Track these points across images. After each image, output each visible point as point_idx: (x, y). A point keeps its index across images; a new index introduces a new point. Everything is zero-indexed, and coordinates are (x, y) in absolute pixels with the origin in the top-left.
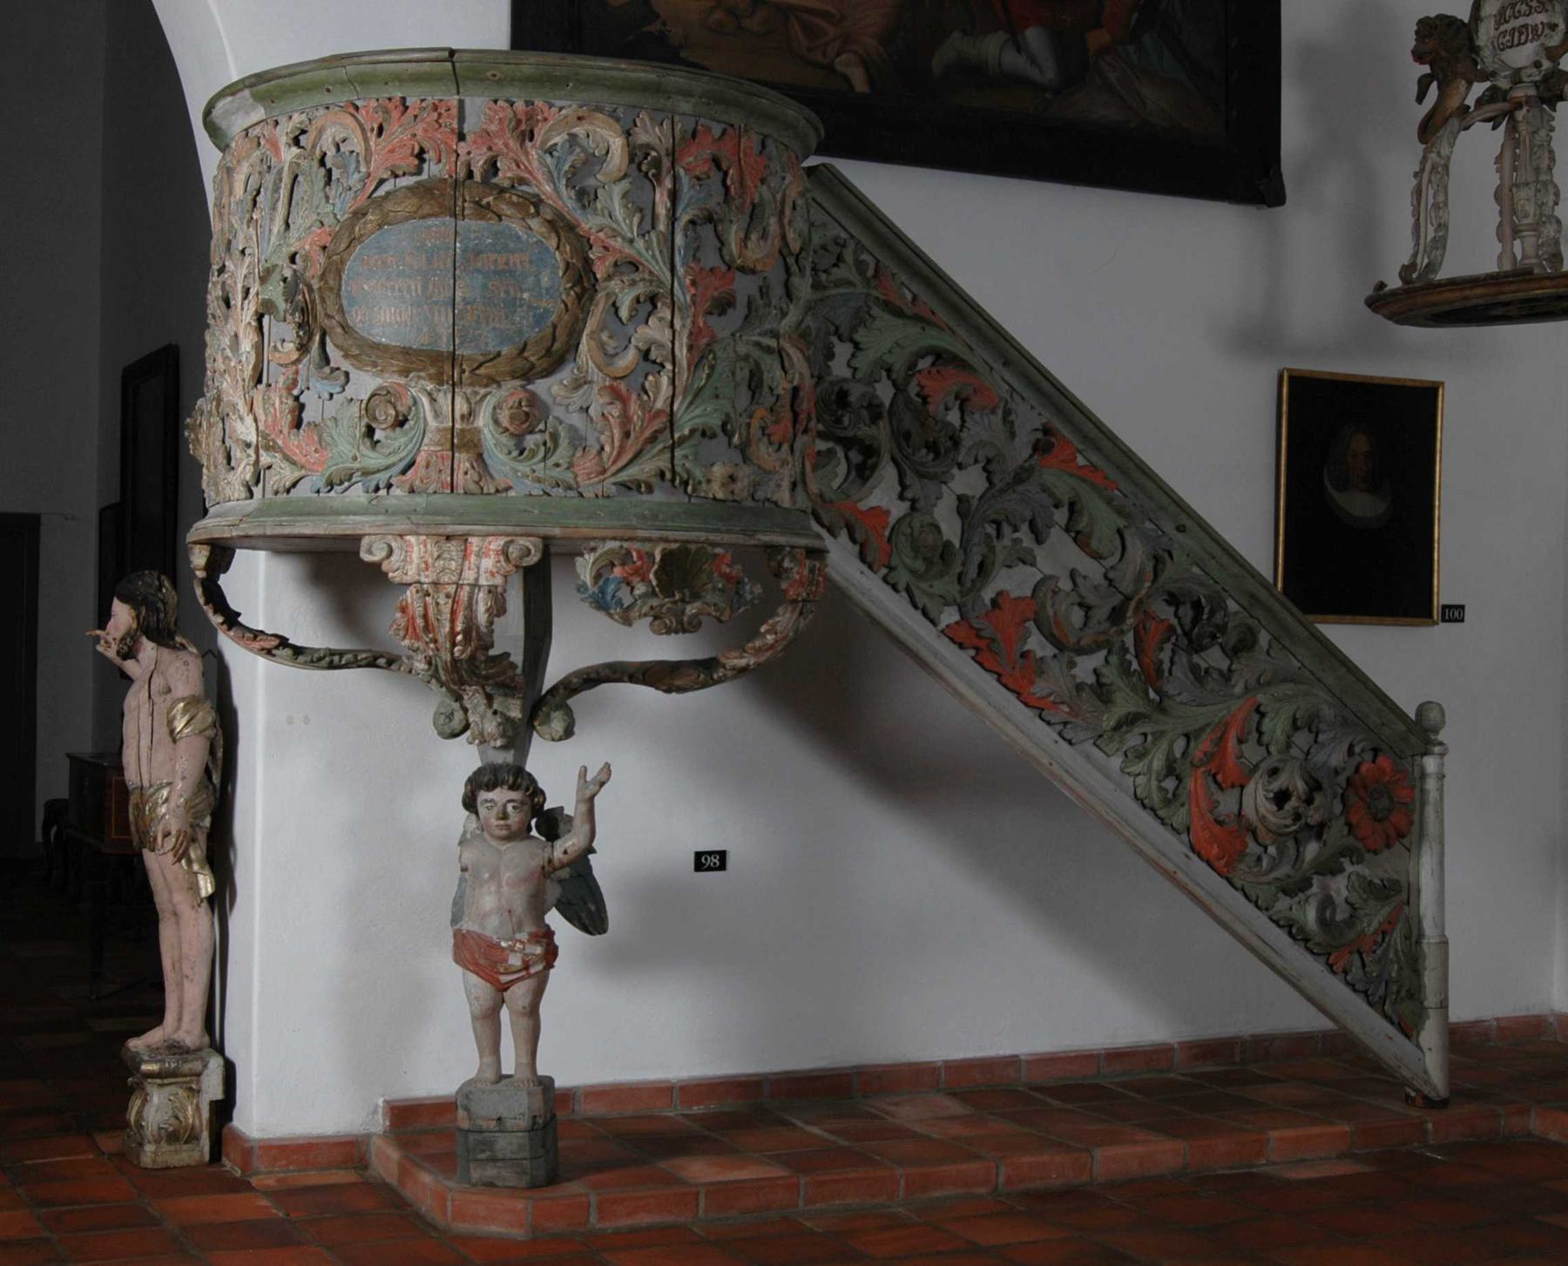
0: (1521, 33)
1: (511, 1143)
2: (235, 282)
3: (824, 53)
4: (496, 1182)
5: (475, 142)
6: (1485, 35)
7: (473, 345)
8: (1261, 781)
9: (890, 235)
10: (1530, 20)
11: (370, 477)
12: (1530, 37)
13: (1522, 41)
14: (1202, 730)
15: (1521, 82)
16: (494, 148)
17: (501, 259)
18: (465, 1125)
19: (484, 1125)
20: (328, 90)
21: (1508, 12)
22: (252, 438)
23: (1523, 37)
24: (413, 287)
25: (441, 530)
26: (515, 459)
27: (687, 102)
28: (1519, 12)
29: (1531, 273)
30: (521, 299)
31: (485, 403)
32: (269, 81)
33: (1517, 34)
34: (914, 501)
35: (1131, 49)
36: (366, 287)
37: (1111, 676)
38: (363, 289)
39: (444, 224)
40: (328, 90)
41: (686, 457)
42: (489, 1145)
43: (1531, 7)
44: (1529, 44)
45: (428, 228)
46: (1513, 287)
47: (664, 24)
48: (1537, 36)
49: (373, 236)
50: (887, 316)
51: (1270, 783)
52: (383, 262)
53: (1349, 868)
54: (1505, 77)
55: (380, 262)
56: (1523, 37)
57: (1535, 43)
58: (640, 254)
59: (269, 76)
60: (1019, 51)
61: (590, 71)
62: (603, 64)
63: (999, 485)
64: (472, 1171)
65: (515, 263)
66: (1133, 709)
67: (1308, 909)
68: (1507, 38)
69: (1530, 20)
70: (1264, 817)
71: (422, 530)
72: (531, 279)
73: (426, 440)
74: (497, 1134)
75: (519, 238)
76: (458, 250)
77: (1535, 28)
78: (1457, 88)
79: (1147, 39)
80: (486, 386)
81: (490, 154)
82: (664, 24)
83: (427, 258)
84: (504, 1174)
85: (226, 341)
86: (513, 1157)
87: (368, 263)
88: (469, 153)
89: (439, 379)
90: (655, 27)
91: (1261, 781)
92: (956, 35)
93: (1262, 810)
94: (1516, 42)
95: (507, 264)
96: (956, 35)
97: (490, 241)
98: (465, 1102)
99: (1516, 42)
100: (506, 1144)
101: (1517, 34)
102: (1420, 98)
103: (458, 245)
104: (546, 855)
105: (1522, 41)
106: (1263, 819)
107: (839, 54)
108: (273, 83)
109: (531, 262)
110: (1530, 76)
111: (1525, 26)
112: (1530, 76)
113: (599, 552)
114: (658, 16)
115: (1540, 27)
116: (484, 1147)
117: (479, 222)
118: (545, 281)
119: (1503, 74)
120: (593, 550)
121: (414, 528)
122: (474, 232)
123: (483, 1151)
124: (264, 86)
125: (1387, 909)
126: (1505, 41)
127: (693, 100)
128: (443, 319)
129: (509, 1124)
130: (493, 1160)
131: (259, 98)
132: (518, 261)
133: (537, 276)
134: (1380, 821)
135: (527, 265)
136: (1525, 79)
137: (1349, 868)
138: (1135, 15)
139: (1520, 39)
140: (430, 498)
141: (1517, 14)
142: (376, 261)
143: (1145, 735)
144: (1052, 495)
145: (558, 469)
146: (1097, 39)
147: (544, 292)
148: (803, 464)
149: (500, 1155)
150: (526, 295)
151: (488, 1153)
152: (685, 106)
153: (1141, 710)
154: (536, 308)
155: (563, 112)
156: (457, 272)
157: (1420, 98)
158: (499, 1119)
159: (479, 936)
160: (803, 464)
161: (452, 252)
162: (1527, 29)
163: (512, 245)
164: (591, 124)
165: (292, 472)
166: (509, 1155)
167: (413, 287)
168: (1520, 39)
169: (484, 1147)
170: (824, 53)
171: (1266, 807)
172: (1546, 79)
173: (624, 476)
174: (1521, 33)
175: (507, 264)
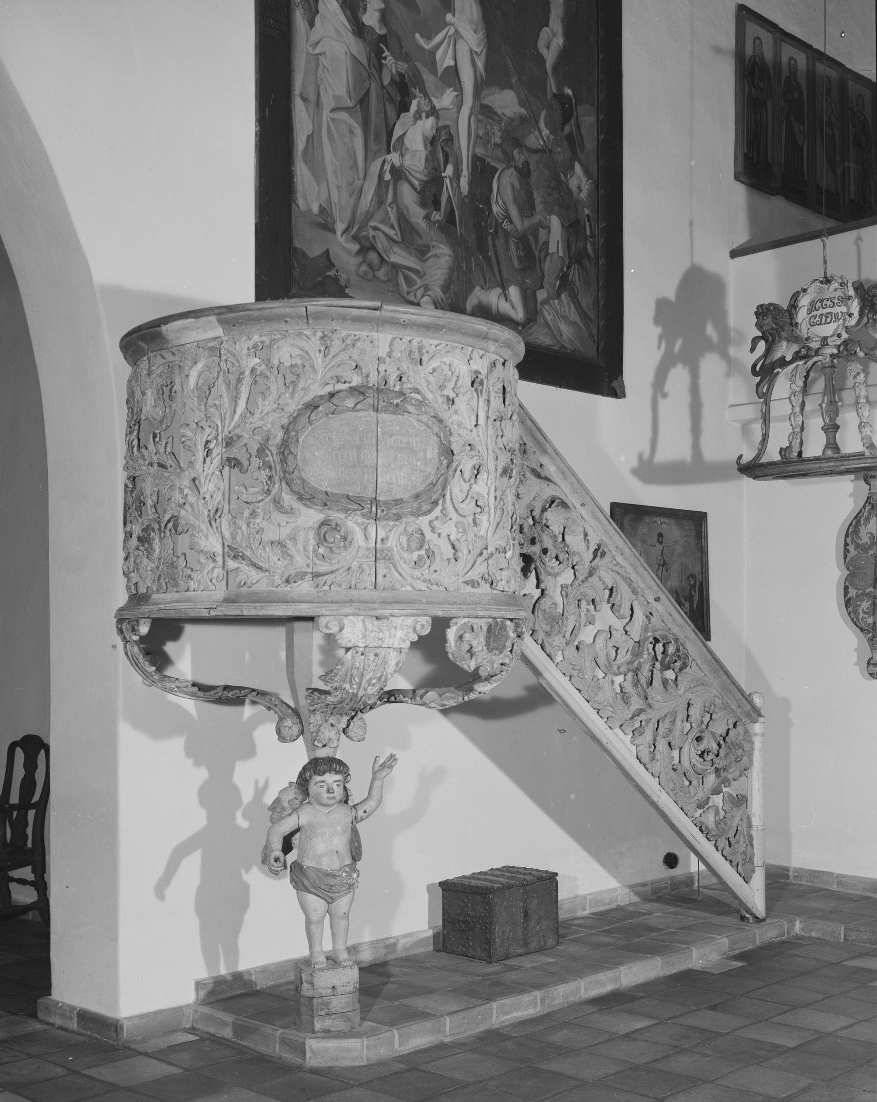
0: (827, 317)
1: (340, 1003)
2: (195, 444)
3: (415, 296)
4: (331, 1029)
5: (390, 364)
6: (802, 316)
7: (387, 494)
8: (692, 744)
10: (833, 310)
11: (320, 578)
12: (834, 319)
13: (828, 321)
14: (666, 716)
15: (828, 344)
16: (401, 369)
17: (405, 440)
19: (323, 992)
20: (286, 322)
21: (818, 305)
22: (218, 549)
23: (829, 320)
24: (351, 456)
25: (374, 613)
27: (494, 345)
28: (826, 305)
29: (864, 455)
30: (417, 466)
31: (393, 531)
33: (824, 318)
35: (556, 301)
36: (317, 454)
37: (629, 688)
38: (314, 455)
39: (370, 415)
41: (493, 565)
42: (327, 1005)
43: (834, 303)
44: (832, 324)
47: (337, 271)
48: (837, 319)
49: (321, 421)
51: (698, 745)
52: (329, 439)
54: (816, 342)
55: (327, 439)
56: (829, 320)
57: (836, 324)
58: (474, 439)
64: (315, 1023)
65: (412, 443)
66: (639, 707)
67: (709, 815)
69: (833, 310)
70: (694, 765)
72: (422, 453)
73: (360, 555)
74: (332, 997)
76: (379, 433)
77: (836, 315)
78: (782, 346)
79: (563, 297)
82: (337, 271)
83: (360, 437)
85: (186, 482)
86: (342, 1011)
87: (318, 439)
88: (386, 371)
90: (332, 273)
91: (692, 744)
93: (694, 761)
94: (823, 322)
95: (408, 443)
96: (478, 288)
97: (397, 428)
98: (310, 978)
99: (823, 322)
100: (337, 1004)
101: (824, 318)
102: (752, 350)
103: (379, 430)
104: (354, 815)
105: (828, 321)
106: (693, 766)
108: (241, 313)
109: (421, 442)
110: (833, 341)
111: (830, 313)
112: (833, 341)
113: (459, 624)
114: (333, 265)
116: (323, 1007)
117: (391, 415)
118: (429, 456)
119: (815, 340)
122: (389, 421)
123: (323, 1009)
125: (741, 812)
126: (815, 321)
127: (497, 344)
129: (340, 990)
130: (329, 1014)
131: (223, 322)
132: (414, 442)
133: (425, 451)
135: (419, 444)
136: (830, 343)
137: (725, 790)
138: (558, 283)
139: (826, 320)
140: (360, 592)
141: (824, 306)
142: (325, 437)
143: (641, 722)
145: (436, 574)
146: (542, 295)
147: (428, 461)
150: (419, 463)
152: (492, 348)
153: (642, 707)
154: (424, 472)
155: (438, 348)
157: (752, 350)
158: (333, 987)
159: (317, 870)
161: (375, 433)
163: (410, 431)
165: (257, 574)
166: (340, 1010)
167: (351, 456)
168: (826, 320)
169: (323, 1007)
170: (415, 296)
173: (467, 578)
174: (827, 317)
175: (408, 443)
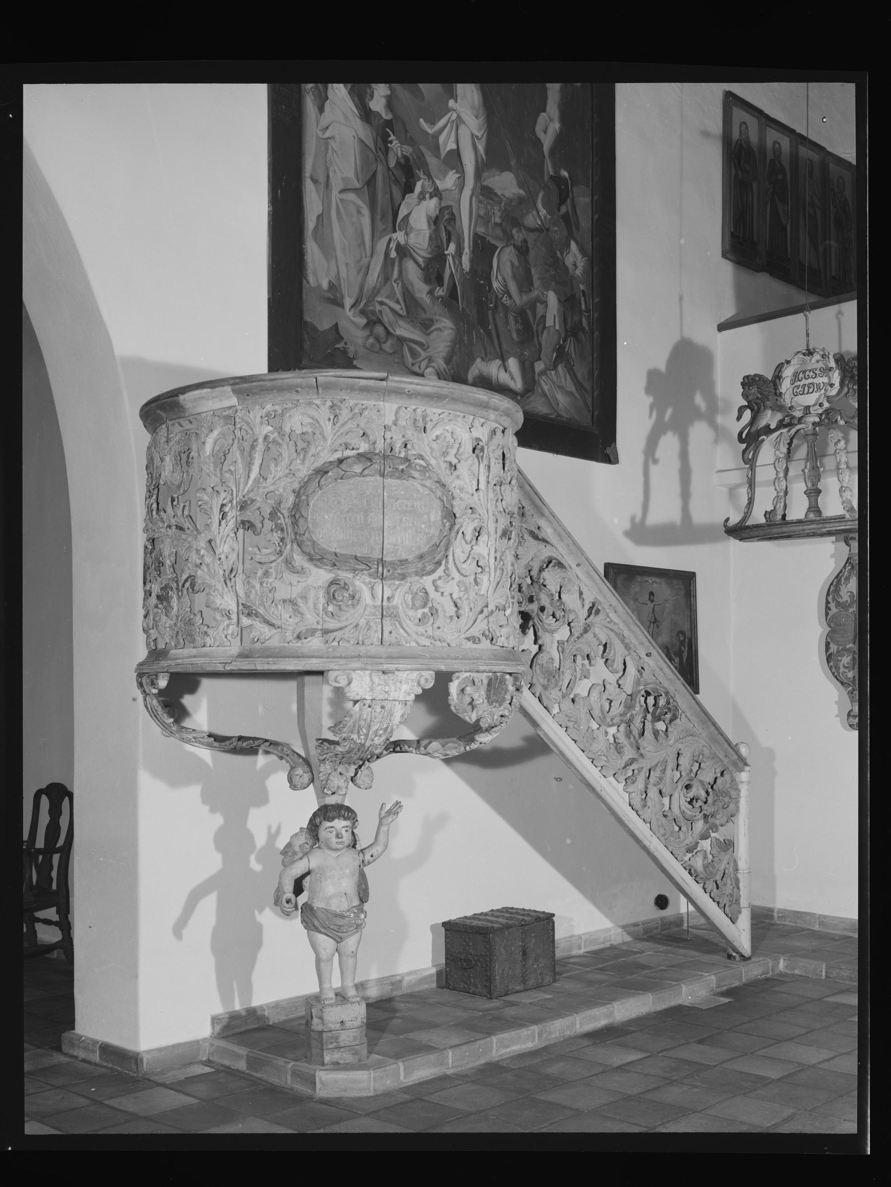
0: (809, 388)
3: (419, 367)
4: (340, 1062)
9: (532, 492)
10: (815, 381)
16: (406, 436)
18: (320, 1028)
19: (333, 1026)
20: (297, 391)
21: (801, 375)
23: (811, 390)
24: (358, 518)
26: (416, 624)
28: (808, 376)
29: (844, 518)
30: (421, 528)
32: (252, 382)
33: (806, 388)
34: (540, 647)
35: (553, 372)
36: (326, 517)
40: (297, 391)
42: (336, 1039)
43: (816, 374)
44: (814, 394)
45: (368, 482)
46: (832, 525)
47: (346, 344)
48: (819, 389)
50: (531, 539)
51: (688, 793)
52: (338, 502)
53: (713, 835)
54: (799, 410)
55: (336, 503)
56: (811, 390)
57: (818, 394)
59: (254, 379)
60: (506, 371)
61: (413, 386)
62: (415, 381)
63: (577, 634)
64: (325, 1056)
68: (800, 389)
69: (815, 381)
71: (369, 667)
72: (426, 516)
75: (418, 491)
76: (385, 497)
77: (818, 385)
78: (766, 415)
79: (560, 368)
80: (375, 579)
81: (403, 439)
82: (346, 344)
84: (344, 1055)
86: (350, 1044)
89: (375, 575)
90: (340, 345)
91: (682, 792)
92: (479, 360)
93: (683, 808)
95: (413, 506)
100: (345, 1038)
102: (739, 418)
103: (385, 494)
106: (683, 813)
107: (426, 368)
108: (254, 384)
110: (816, 410)
111: (813, 384)
112: (816, 410)
114: (342, 338)
115: (822, 385)
116: (332, 1041)
118: (433, 519)
120: (458, 677)
121: (364, 666)
123: (332, 1043)
124: (246, 385)
126: (798, 391)
128: (377, 539)
130: (339, 1048)
133: (429, 514)
134: (725, 808)
136: (812, 412)
137: (713, 835)
139: (809, 390)
142: (334, 501)
143: (633, 770)
144: (598, 639)
145: (439, 630)
146: (539, 366)
148: (406, 631)
149: (342, 1044)
150: (423, 526)
151: (335, 1044)
156: (385, 510)
157: (739, 418)
158: (342, 1022)
160: (406, 631)
161: (382, 497)
162: (814, 386)
163: (415, 495)
164: (455, 424)
168: (809, 390)
169: (332, 1041)
170: (419, 367)
171: (686, 806)
172: (827, 412)
173: (468, 634)
174: (809, 388)
175: (413, 506)
